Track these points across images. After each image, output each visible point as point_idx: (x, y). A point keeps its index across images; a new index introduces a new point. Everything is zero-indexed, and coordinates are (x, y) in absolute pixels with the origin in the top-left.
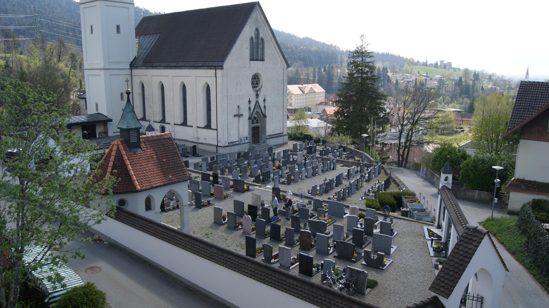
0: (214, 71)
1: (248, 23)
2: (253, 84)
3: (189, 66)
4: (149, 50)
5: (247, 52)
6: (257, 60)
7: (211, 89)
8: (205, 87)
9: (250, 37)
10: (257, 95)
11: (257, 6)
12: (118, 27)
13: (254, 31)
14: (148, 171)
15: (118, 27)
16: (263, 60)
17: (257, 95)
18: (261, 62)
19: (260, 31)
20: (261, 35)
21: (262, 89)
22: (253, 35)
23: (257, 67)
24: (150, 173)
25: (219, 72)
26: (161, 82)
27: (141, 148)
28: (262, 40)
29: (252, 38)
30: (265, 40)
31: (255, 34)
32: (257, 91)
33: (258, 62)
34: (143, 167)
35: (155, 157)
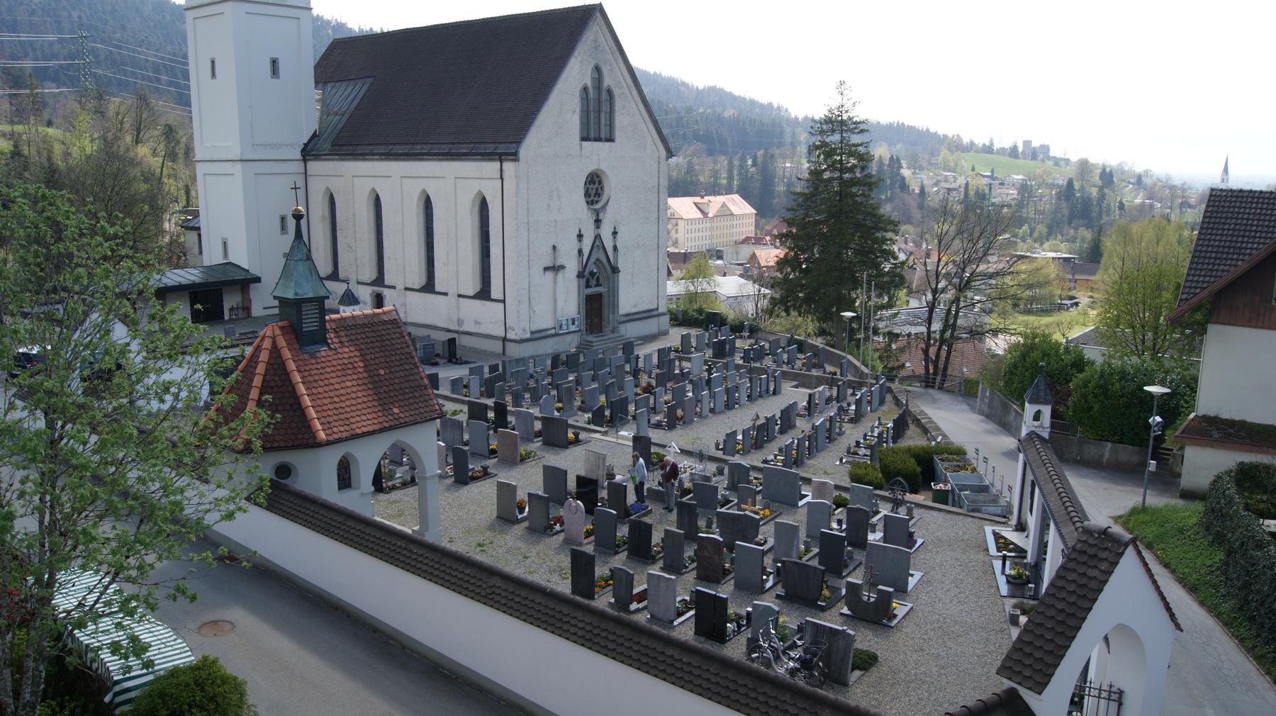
0: (496, 165)
1: (576, 53)
2: (587, 194)
3: (438, 154)
4: (346, 117)
5: (575, 122)
6: (598, 139)
7: (490, 207)
8: (478, 203)
9: (580, 87)
10: (598, 222)
11: (598, 14)
12: (274, 62)
13: (590, 72)
14: (343, 398)
15: (274, 62)
16: (610, 139)
17: (598, 222)
18: (608, 144)
19: (605, 71)
20: (607, 82)
21: (609, 207)
22: (589, 82)
23: (597, 155)
24: (348, 403)
25: (509, 166)
26: (374, 190)
27: (328, 345)
28: (609, 92)
29: (585, 89)
30: (616, 92)
31: (593, 78)
32: (597, 212)
33: (600, 144)
34: (331, 388)
35: (361, 364)
